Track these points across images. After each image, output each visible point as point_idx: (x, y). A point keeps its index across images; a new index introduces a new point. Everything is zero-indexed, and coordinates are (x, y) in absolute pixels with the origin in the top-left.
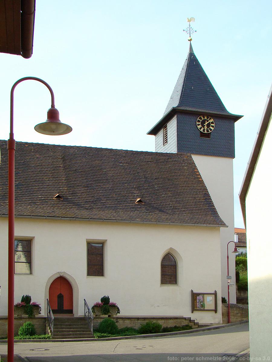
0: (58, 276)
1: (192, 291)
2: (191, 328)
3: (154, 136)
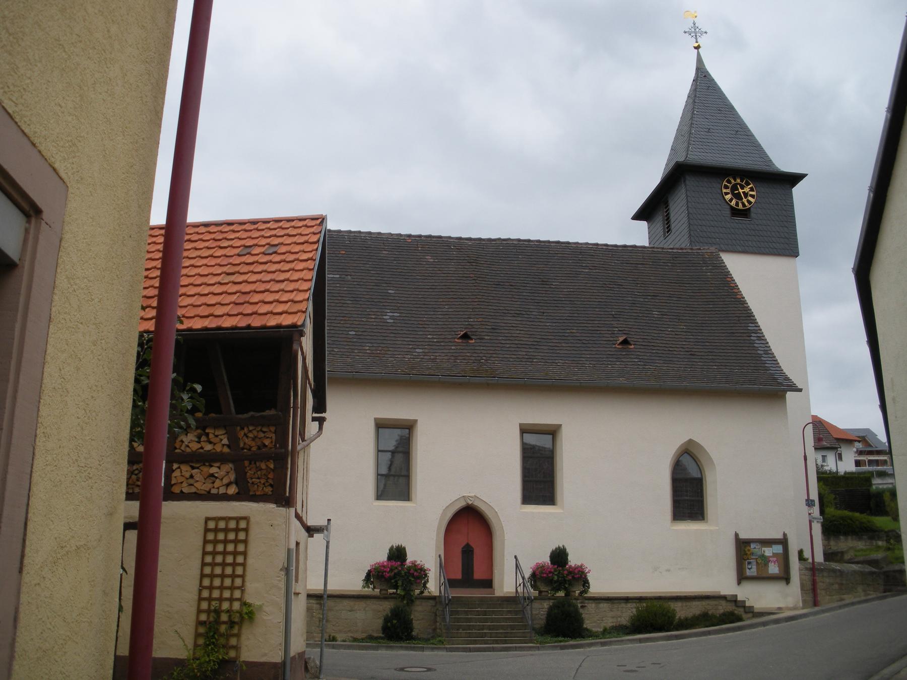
0: (462, 504)
1: (737, 535)
2: (740, 619)
3: (645, 223)
